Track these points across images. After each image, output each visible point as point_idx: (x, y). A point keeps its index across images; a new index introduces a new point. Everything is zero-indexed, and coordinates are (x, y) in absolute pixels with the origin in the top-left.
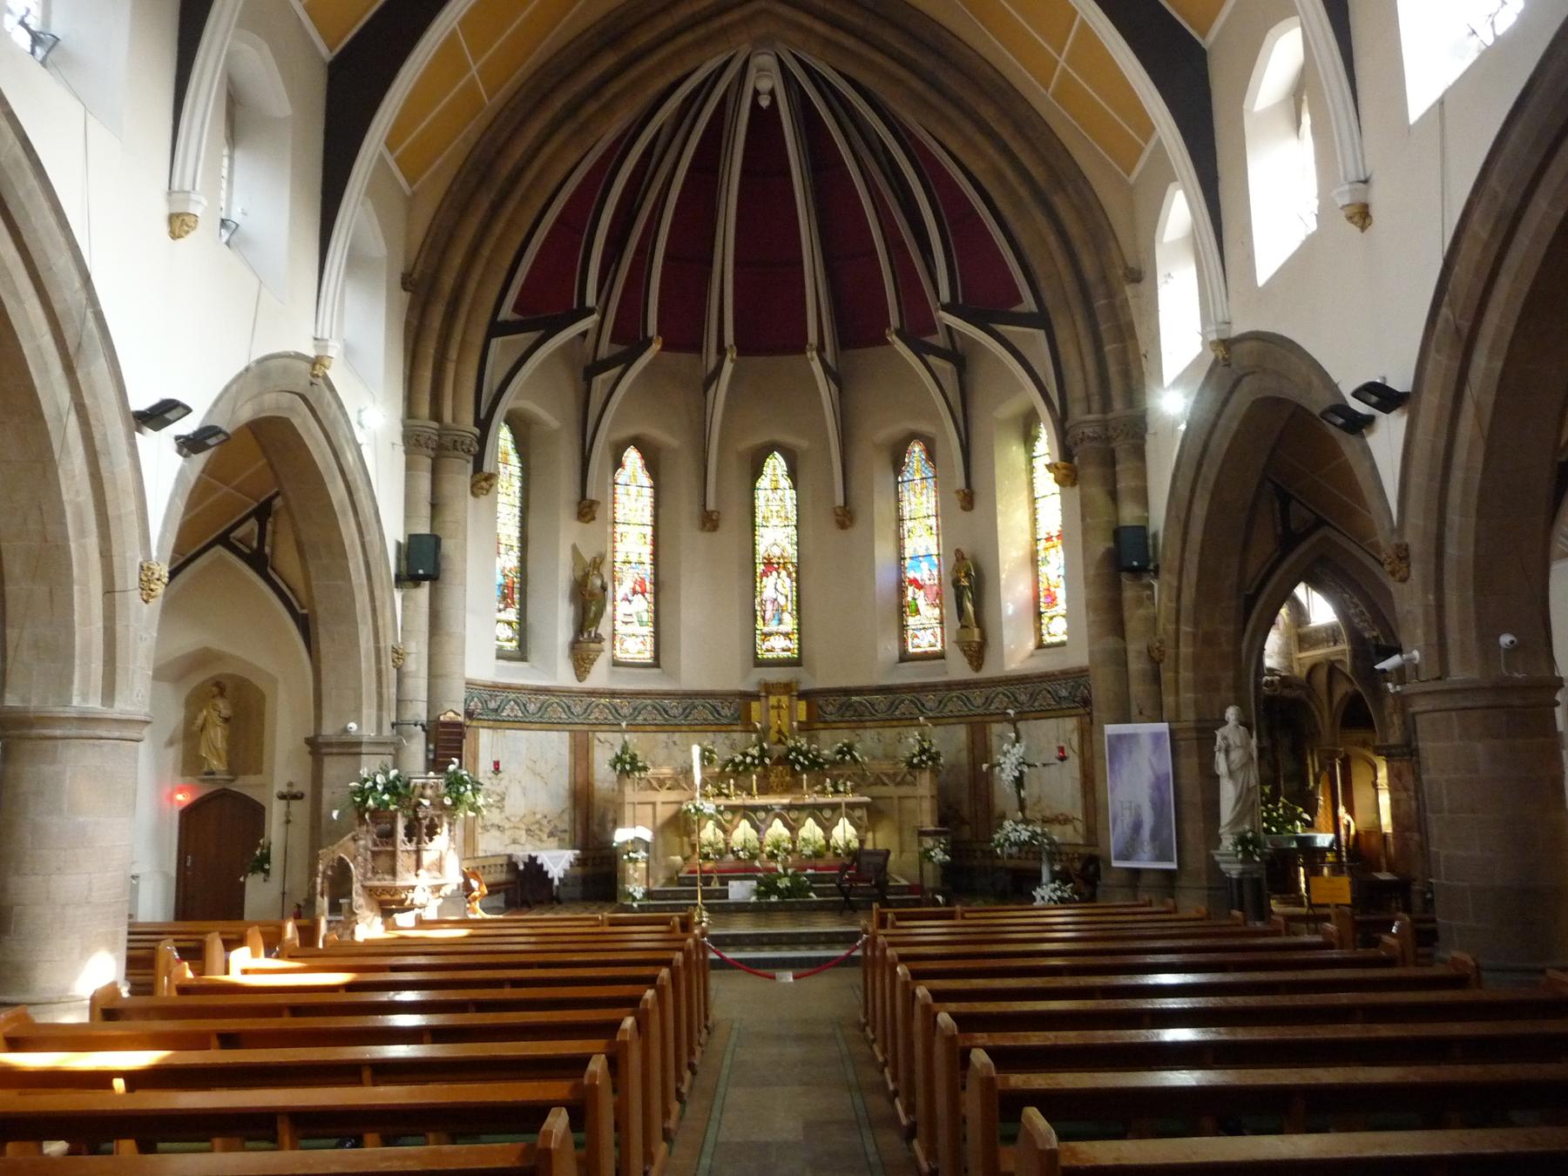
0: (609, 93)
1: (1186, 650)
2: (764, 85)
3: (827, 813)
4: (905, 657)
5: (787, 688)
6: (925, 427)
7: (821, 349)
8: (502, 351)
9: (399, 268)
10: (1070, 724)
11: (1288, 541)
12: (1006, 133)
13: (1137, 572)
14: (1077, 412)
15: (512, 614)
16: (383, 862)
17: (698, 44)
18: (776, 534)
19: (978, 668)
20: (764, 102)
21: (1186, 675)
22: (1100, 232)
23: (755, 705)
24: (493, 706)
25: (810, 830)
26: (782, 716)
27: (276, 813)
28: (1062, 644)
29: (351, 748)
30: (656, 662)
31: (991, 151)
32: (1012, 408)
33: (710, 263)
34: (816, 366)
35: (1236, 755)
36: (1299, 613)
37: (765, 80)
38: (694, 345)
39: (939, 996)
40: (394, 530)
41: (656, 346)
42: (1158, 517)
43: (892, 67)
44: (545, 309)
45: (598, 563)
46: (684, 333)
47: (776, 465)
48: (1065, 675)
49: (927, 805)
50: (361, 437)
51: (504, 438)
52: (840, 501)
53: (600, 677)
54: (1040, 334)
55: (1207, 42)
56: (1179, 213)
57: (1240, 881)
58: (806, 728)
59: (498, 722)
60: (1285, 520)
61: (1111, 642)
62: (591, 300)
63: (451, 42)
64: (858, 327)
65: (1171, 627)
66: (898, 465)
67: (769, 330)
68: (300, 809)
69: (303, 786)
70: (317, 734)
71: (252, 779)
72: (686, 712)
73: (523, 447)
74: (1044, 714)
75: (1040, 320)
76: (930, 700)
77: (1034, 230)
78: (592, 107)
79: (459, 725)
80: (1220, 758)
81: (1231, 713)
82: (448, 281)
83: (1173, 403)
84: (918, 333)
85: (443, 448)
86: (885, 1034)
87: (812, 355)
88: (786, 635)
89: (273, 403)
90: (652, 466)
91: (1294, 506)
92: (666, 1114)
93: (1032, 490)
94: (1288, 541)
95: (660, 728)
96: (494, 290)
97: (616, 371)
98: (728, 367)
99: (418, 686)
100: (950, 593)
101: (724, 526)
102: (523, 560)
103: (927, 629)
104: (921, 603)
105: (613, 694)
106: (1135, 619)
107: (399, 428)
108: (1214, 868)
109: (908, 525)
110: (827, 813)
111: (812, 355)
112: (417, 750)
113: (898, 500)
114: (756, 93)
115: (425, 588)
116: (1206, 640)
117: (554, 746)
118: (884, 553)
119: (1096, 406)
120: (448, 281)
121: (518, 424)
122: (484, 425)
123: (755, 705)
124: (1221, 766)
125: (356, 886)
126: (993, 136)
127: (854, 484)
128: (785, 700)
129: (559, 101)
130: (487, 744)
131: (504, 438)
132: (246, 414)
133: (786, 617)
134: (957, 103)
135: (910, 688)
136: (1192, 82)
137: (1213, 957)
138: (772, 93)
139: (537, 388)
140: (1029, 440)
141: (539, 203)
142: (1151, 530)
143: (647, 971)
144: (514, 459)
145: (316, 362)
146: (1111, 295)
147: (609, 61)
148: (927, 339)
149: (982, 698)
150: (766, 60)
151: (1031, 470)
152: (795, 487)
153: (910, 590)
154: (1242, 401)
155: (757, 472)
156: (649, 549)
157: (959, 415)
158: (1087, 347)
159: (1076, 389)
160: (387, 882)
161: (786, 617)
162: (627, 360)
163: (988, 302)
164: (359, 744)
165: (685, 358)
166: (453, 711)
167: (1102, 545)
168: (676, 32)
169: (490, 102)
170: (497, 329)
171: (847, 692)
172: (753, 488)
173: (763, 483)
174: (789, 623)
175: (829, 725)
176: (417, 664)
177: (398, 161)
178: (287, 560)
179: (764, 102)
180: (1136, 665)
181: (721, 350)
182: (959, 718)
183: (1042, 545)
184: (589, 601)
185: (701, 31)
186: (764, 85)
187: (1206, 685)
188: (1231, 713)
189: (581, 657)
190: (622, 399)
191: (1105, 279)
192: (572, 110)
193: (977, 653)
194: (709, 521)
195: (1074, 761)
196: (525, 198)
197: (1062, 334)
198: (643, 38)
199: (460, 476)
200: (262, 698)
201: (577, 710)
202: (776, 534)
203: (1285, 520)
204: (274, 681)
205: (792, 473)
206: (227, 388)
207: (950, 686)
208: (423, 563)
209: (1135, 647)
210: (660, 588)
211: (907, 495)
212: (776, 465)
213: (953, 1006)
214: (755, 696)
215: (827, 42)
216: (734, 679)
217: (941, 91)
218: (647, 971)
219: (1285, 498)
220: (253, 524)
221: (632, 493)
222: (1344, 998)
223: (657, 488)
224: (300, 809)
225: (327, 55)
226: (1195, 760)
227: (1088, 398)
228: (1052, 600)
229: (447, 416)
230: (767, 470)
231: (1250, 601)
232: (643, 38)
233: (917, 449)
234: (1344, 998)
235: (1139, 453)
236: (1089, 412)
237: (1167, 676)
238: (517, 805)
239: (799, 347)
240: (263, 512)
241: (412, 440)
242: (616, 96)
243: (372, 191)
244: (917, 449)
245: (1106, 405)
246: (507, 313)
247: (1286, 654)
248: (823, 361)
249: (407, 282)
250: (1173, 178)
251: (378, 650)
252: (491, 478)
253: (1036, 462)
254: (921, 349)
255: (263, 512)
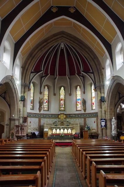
0: (45, 47)
1: (109, 110)
2: (62, 46)
3: (68, 128)
4: (77, 110)
5: (63, 114)
6: (79, 84)
7: (68, 75)
8: (32, 75)
9: (21, 66)
10: (96, 118)
11: (120, 98)
12: (89, 52)
13: (103, 102)
14: (97, 83)
15: (32, 105)
16: (18, 133)
17: (55, 42)
18: (62, 96)
19: (85, 112)
20: (62, 48)
21: (109, 113)
22: (99, 64)
23: (59, 116)
24: (30, 115)
25: (66, 130)
26: (62, 117)
27: (6, 126)
28: (95, 109)
29: (14, 120)
30: (48, 110)
31: (88, 55)
32: (89, 83)
33: (56, 65)
34: (67, 77)
35: (114, 122)
36: (121, 106)
37: (62, 46)
38: (54, 75)
39: (80, 148)
40: (20, 95)
41: (49, 75)
42: (106, 96)
43: (76, 45)
44: (37, 70)
45: (42, 99)
46: (53, 73)
47: (62, 88)
48: (95, 113)
49: (79, 127)
50: (16, 85)
51: (32, 85)
52: (70, 93)
53: (42, 112)
54: (93, 75)
55: (111, 44)
56: (108, 62)
57: (114, 136)
58: (65, 118)
59: (31, 117)
60: (120, 96)
61: (100, 109)
62: (42, 69)
63: (28, 42)
64: (72, 73)
65: (107, 108)
66: (76, 88)
67: (62, 73)
68: (8, 126)
69: (9, 123)
70: (10, 118)
71: (3, 123)
72: (52, 116)
73: (34, 86)
74: (93, 117)
75: (93, 73)
76: (80, 115)
77: (92, 63)
78: (43, 49)
79: (26, 117)
80: (112, 123)
81: (114, 118)
82: (26, 68)
83: (107, 83)
84: (79, 74)
85: (25, 87)
86: (79, 161)
87: (67, 76)
88: (63, 108)
89: (7, 81)
90: (48, 88)
91: (121, 95)
92: (48, 174)
93: (91, 92)
94: (120, 98)
95: (48, 118)
96: (31, 68)
97: (35, 73)
98: (57, 77)
99: (21, 113)
100: (82, 103)
101: (56, 96)
102: (33, 98)
103: (79, 107)
104: (79, 104)
105: (43, 114)
106: (103, 107)
107: (20, 84)
108: (111, 135)
109: (77, 95)
110: (68, 128)
111: (67, 76)
112: (21, 121)
113: (76, 93)
114: (61, 47)
115: (23, 101)
116: (111, 109)
117: (37, 120)
118: (75, 99)
119: (99, 83)
120: (26, 68)
121: (34, 83)
122: (30, 83)
123: (59, 116)
124: (112, 124)
125: (14, 135)
126: (87, 53)
127: (71, 92)
128: (63, 115)
129: (40, 48)
130: (29, 119)
131: (32, 85)
132: (4, 82)
133: (63, 106)
134: (84, 50)
135: (77, 114)
136: (109, 48)
137: (110, 145)
138: (63, 47)
139: (36, 79)
140: (91, 86)
141: (37, 59)
142: (105, 97)
143: (48, 149)
144: (33, 87)
145: (12, 76)
146: (101, 70)
147: (45, 43)
148: (80, 75)
149: (85, 116)
150: (62, 44)
151: (91, 89)
152: (64, 91)
153: (77, 103)
154: (115, 83)
155: (60, 89)
156: (48, 97)
157: (83, 83)
158: (98, 78)
159: (97, 81)
160: (18, 135)
161: (63, 106)
162: (46, 76)
163: (87, 71)
164: (15, 119)
165: (52, 76)
166: (26, 116)
167: (99, 98)
168: (53, 41)
169: (32, 48)
170: (32, 72)
171: (70, 114)
172: (60, 91)
173: (61, 90)
174: (63, 106)
175: (68, 118)
176: (21, 110)
177: (13, 38)
178: (8, 98)
179: (62, 48)
180: (103, 112)
181: (57, 75)
182: (83, 118)
183: (92, 98)
184: (41, 103)
185: (56, 41)
186: (62, 46)
187: (111, 114)
188: (114, 118)
189: (40, 110)
190: (46, 82)
191: (100, 69)
192: (41, 49)
193: (85, 110)
194: (55, 95)
195: (96, 123)
196: (35, 58)
197: (95, 75)
198: (49, 41)
199: (27, 89)
200: (4, 114)
201: (39, 116)
202: (62, 96)
203: (120, 96)
204: (6, 112)
205: (80, 88)
206: (2, 79)
207: (82, 114)
208: (23, 100)
209: (103, 110)
210: (49, 102)
211: (77, 92)
212: (62, 88)
213: (82, 149)
214: (59, 115)
215: (70, 42)
216: (57, 112)
217: (82, 48)
218: (48, 149)
219: (119, 93)
220: (4, 94)
221: (46, 92)
222: (121, 148)
223: (49, 91)
224: (8, 126)
225: (15, 43)
226: (109, 123)
227: (98, 82)
228: (94, 104)
229: (26, 83)
230: (61, 89)
231: (116, 105)
232: (49, 41)
233: (78, 87)
234: (121, 148)
235: (104, 88)
236: (33, 109)
237: (106, 113)
238: (32, 127)
239: (66, 75)
240: (5, 93)
241: (22, 85)
242: (46, 47)
243: (19, 58)
244: (78, 87)
245: (100, 83)
246: (33, 71)
247: (119, 111)
248: (68, 77)
249: (22, 67)
250: (107, 58)
251: (17, 109)
252: (30, 89)
253: (92, 89)
254: (79, 76)
255: (5, 93)
